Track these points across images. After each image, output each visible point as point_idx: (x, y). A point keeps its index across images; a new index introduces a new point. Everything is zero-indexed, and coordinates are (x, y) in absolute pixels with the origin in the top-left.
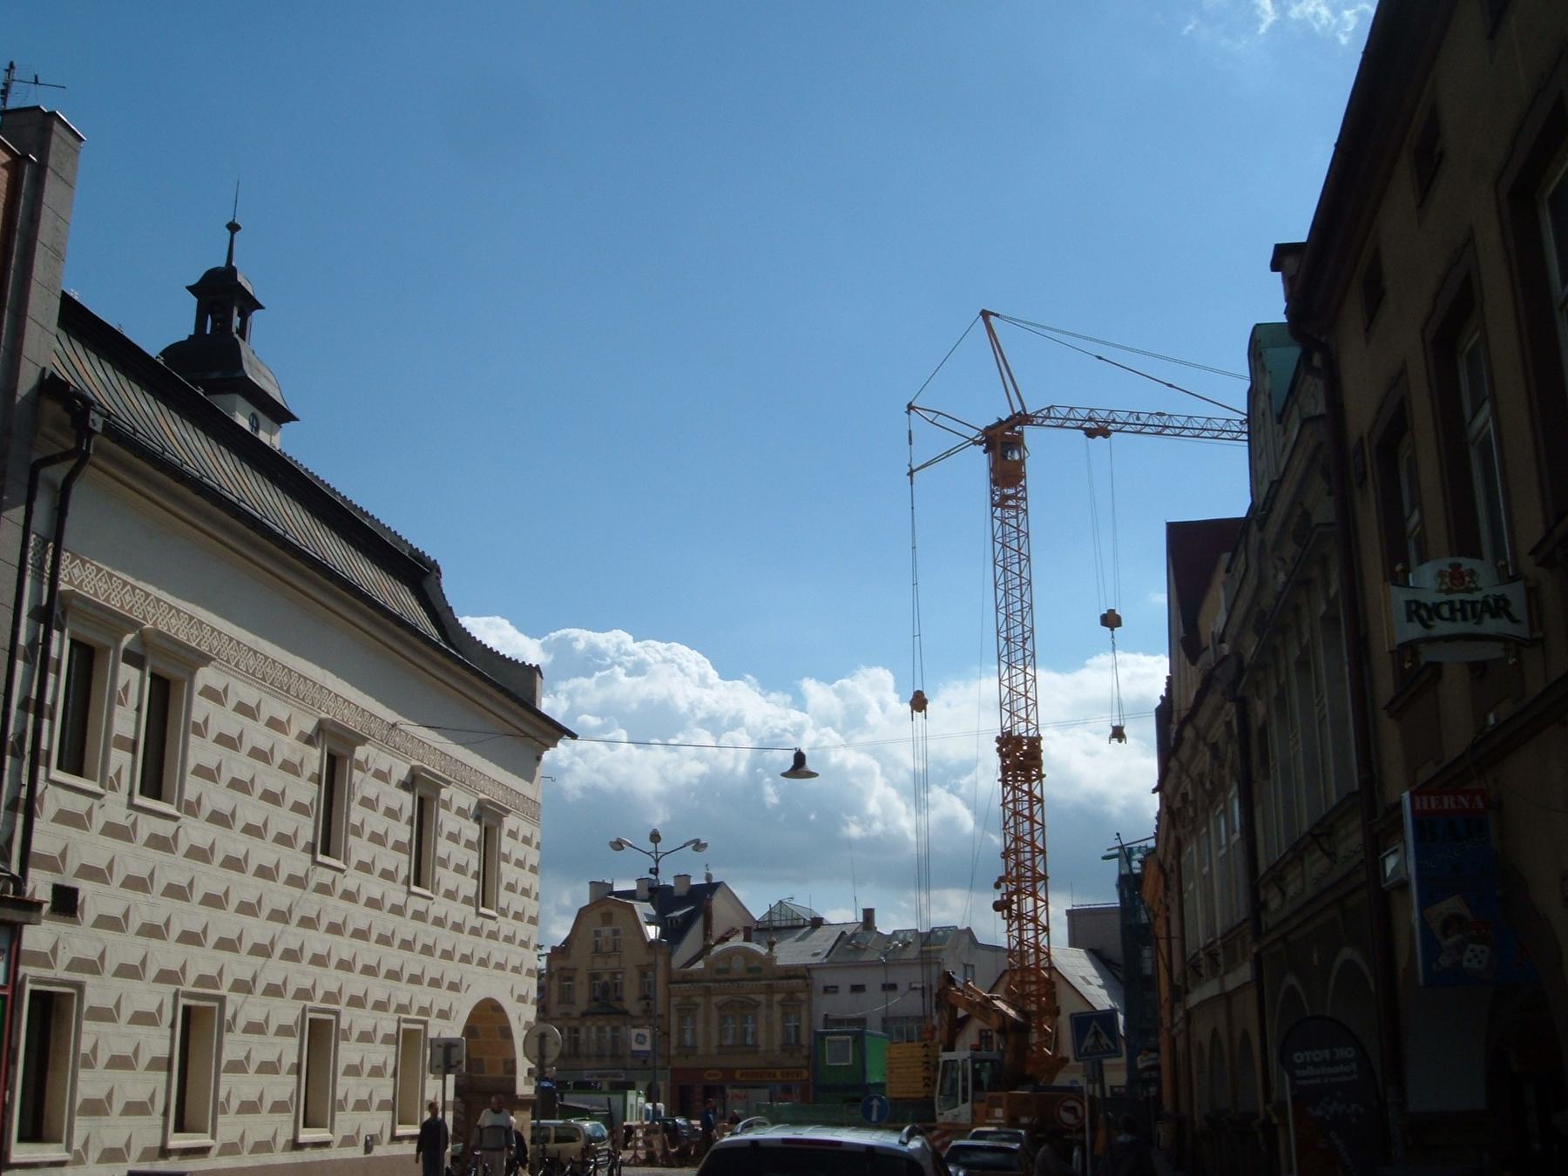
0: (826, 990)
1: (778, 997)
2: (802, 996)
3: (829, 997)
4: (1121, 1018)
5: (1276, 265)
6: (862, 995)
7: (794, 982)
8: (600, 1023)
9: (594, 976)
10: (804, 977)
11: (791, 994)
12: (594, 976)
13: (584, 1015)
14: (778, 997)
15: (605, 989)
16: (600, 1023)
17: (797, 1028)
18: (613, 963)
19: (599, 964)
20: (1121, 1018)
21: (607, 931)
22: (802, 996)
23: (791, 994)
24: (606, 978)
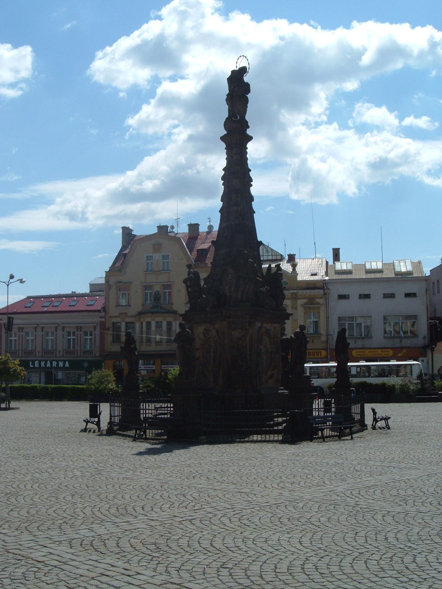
0: (342, 297)
1: (300, 302)
2: (321, 301)
3: (343, 302)
4: (272, 423)
5: (160, 228)
6: (367, 301)
7: (316, 291)
8: (159, 319)
9: (147, 287)
10: (323, 288)
11: (311, 301)
12: (147, 287)
13: (140, 314)
14: (300, 302)
15: (157, 297)
16: (159, 319)
17: (316, 324)
18: (163, 278)
19: (151, 279)
20: (272, 423)
21: (157, 256)
22: (321, 301)
23: (311, 301)
24: (157, 288)
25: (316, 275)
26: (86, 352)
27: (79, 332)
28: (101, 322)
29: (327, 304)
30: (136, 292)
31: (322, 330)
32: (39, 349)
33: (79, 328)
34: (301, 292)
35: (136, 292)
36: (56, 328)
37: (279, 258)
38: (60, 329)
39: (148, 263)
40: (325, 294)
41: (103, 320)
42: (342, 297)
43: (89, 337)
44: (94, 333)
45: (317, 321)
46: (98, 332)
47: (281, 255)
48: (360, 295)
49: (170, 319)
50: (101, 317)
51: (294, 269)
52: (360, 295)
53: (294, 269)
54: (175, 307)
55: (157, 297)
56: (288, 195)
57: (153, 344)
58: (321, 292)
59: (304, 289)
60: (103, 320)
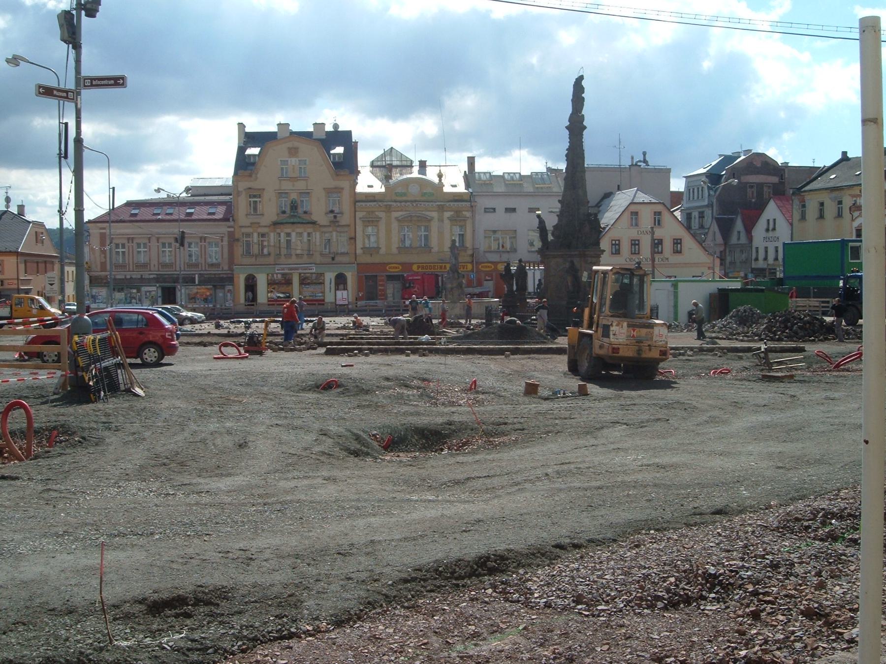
0: (487, 210)
1: (447, 214)
2: (468, 214)
6: (513, 214)
7: (464, 203)
10: (470, 201)
11: (458, 212)
12: (281, 194)
13: (275, 224)
14: (447, 214)
17: (462, 236)
18: (301, 185)
19: (287, 186)
21: (293, 161)
22: (468, 214)
23: (458, 212)
24: (294, 196)
25: (455, 186)
26: (212, 265)
27: (203, 243)
28: (101, 233)
29: (473, 216)
30: (270, 200)
31: (468, 244)
32: (154, 262)
33: (131, 239)
34: (448, 204)
35: (270, 200)
36: (149, 239)
37: (409, 164)
38: (154, 240)
39: (282, 169)
40: (472, 206)
41: (232, 229)
42: (487, 210)
43: (167, 249)
44: (127, 245)
45: (463, 235)
46: (225, 243)
47: (412, 161)
48: (506, 209)
49: (310, 230)
50: (229, 227)
51: (440, 180)
52: (506, 209)
53: (440, 180)
54: (314, 218)
55: (294, 206)
56: (752, 163)
57: (294, 257)
58: (468, 204)
59: (451, 201)
60: (232, 229)
